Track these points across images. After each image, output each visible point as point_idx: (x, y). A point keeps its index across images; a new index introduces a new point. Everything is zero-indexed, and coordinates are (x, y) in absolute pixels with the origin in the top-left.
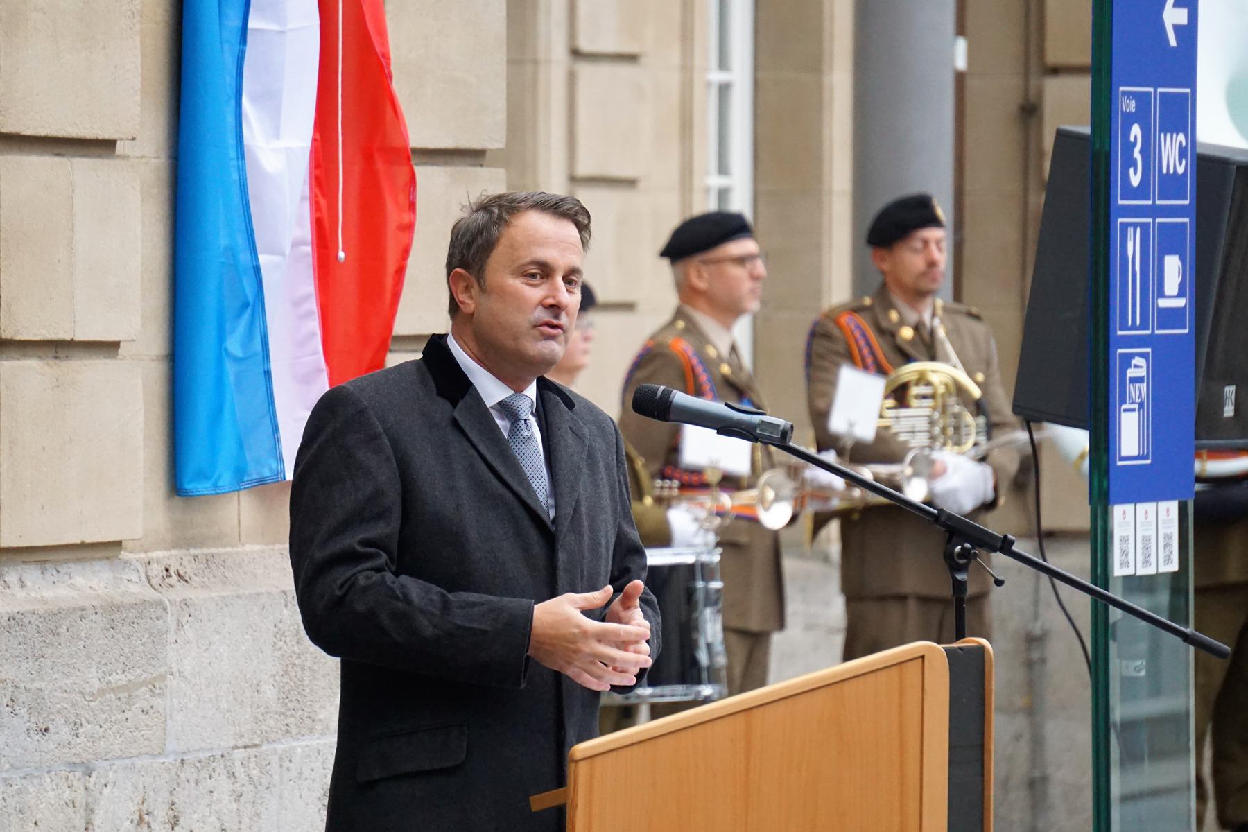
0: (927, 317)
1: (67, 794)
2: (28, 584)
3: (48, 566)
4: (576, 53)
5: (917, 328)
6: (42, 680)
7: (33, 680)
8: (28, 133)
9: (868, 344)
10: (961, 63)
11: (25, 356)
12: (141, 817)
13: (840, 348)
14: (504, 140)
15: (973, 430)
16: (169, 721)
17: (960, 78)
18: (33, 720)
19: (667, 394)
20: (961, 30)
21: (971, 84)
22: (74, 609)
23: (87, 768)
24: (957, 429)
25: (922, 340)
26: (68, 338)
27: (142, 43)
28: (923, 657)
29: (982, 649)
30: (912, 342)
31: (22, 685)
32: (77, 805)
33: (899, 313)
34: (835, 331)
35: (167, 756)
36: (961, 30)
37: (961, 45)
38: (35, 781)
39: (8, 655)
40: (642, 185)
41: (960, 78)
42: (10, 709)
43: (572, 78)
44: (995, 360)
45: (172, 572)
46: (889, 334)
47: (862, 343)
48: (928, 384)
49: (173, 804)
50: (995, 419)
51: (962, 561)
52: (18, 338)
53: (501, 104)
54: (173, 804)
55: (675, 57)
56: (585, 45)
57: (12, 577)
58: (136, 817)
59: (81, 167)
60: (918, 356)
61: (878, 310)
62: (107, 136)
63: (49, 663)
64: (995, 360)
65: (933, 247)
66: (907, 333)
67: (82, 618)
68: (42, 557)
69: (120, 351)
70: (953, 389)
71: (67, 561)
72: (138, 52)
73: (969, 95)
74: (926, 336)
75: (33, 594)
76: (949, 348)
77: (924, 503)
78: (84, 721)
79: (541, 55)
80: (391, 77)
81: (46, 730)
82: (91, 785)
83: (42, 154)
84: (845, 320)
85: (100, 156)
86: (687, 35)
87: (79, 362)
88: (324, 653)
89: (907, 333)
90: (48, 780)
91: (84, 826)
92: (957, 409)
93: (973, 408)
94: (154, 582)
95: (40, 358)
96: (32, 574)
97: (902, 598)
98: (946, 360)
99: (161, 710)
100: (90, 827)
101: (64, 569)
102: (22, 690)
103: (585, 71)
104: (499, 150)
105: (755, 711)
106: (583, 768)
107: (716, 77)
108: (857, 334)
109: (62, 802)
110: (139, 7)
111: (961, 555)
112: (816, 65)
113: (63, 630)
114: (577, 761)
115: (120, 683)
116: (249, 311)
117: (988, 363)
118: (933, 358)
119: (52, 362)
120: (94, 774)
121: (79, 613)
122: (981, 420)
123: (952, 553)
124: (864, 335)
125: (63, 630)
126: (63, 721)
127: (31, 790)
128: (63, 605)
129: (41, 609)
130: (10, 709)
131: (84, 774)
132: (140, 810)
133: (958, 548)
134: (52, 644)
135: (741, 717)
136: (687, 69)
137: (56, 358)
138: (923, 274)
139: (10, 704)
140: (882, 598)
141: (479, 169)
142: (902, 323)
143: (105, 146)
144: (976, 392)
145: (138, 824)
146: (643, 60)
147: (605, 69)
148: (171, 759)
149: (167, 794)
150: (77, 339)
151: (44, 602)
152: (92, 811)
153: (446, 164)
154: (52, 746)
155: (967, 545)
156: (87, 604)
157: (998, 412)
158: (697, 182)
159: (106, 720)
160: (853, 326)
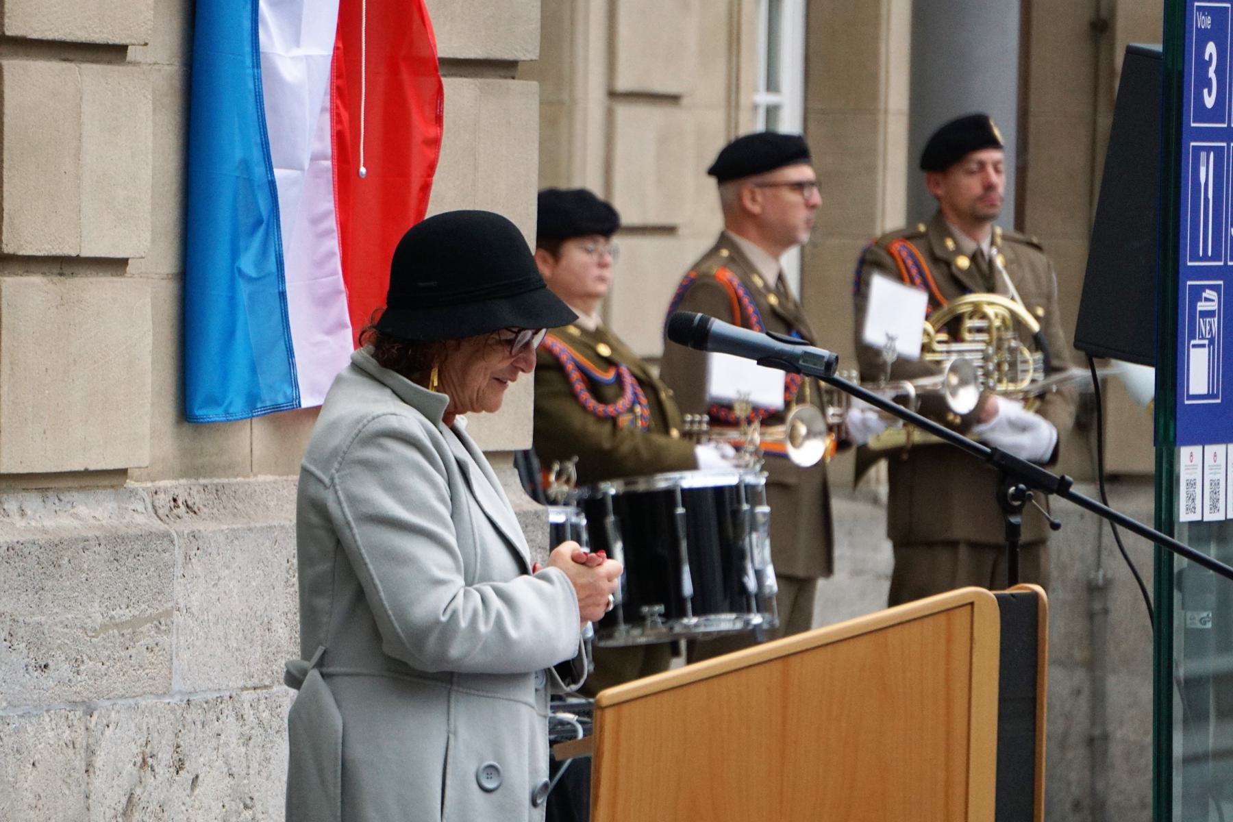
0: (985, 246)
1: (67, 735)
2: (29, 512)
3: (50, 494)
6: (42, 613)
8: (35, 36)
11: (27, 272)
12: (144, 760)
15: (1031, 367)
19: (704, 323)
23: (88, 707)
26: (74, 254)
28: (972, 604)
29: (1035, 596)
30: (968, 272)
31: (21, 619)
32: (77, 746)
35: (172, 696)
38: (34, 720)
39: (7, 586)
40: (684, 101)
50: (1055, 363)
51: (1017, 503)
52: (21, 253)
57: (11, 505)
58: (139, 760)
59: (90, 73)
62: (117, 41)
63: (50, 596)
65: (991, 170)
70: (1009, 322)
71: (69, 489)
74: (985, 267)
75: (33, 523)
78: (85, 658)
81: (46, 666)
82: (92, 726)
83: (49, 59)
84: (897, 247)
85: (109, 62)
89: (963, 262)
90: (48, 719)
91: (84, 768)
92: (1013, 344)
93: (1031, 340)
94: (161, 512)
95: (44, 274)
96: (32, 503)
97: (953, 544)
98: (1004, 292)
100: (91, 770)
101: (66, 497)
106: (609, 716)
111: (1016, 496)
114: (602, 709)
117: (1049, 298)
118: (991, 289)
119: (56, 279)
121: (82, 544)
122: (1039, 356)
123: (1005, 493)
124: (917, 264)
127: (29, 729)
128: (65, 535)
129: (42, 539)
131: (85, 713)
132: (143, 753)
133: (1012, 489)
134: (53, 576)
137: (61, 274)
139: (9, 638)
141: (510, 81)
142: (959, 251)
143: (114, 52)
144: (1035, 326)
148: (177, 698)
151: (46, 532)
153: (475, 75)
154: (52, 684)
155: (1022, 486)
158: (744, 100)
159: (109, 657)
160: (904, 254)
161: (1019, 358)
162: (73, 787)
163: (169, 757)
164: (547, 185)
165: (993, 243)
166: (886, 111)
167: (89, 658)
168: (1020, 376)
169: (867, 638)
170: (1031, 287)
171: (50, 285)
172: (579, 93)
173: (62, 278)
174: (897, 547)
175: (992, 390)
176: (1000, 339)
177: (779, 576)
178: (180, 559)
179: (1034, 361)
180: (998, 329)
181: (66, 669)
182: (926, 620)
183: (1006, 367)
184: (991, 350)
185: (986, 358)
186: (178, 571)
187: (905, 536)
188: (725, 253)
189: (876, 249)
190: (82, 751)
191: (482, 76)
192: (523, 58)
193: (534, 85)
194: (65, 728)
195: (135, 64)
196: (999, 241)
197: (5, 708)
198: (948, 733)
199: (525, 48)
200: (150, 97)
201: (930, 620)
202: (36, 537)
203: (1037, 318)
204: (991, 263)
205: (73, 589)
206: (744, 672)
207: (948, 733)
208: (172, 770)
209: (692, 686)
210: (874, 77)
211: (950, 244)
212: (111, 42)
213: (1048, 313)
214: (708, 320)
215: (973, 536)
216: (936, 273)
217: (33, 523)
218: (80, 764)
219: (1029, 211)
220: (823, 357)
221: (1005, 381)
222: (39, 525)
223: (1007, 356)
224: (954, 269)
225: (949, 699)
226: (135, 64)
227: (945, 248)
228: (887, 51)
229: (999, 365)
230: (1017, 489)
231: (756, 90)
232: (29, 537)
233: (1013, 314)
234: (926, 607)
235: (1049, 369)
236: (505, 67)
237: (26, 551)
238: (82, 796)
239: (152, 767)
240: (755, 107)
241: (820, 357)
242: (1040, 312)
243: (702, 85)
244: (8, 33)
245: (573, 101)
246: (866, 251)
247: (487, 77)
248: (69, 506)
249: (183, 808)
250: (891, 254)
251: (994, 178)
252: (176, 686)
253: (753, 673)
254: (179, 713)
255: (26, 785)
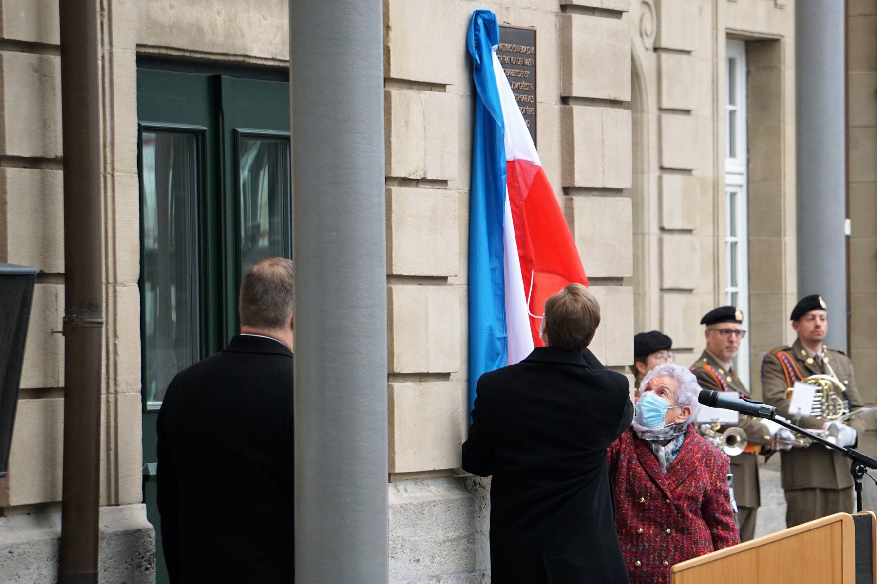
4: (662, 229)
9: (792, 366)
10: (848, 231)
11: (405, 381)
15: (842, 407)
19: (715, 395)
20: (848, 216)
24: (834, 406)
25: (817, 364)
26: (426, 372)
29: (870, 516)
30: (812, 365)
34: (776, 360)
36: (848, 216)
37: (848, 223)
40: (694, 292)
41: (848, 238)
43: (661, 241)
44: (853, 374)
47: (788, 365)
48: (819, 385)
50: (854, 403)
53: (631, 256)
56: (667, 226)
59: (431, 290)
61: (796, 351)
62: (443, 275)
65: (818, 319)
67: (434, 506)
68: (415, 477)
70: (832, 387)
71: (427, 479)
74: (820, 363)
76: (829, 367)
79: (646, 231)
80: (6, 193)
83: (413, 284)
84: (780, 355)
85: (440, 285)
88: (156, 446)
89: (810, 361)
92: (834, 396)
97: (814, 489)
98: (829, 374)
101: (425, 482)
103: (667, 237)
106: (678, 576)
107: (730, 239)
108: (786, 361)
111: (859, 471)
112: (778, 233)
117: (849, 375)
118: (823, 373)
119: (418, 383)
122: (846, 401)
124: (790, 362)
125: (426, 512)
136: (716, 236)
138: (812, 332)
140: (804, 490)
142: (808, 356)
143: (442, 280)
146: (694, 232)
147: (676, 237)
151: (417, 498)
153: (604, 285)
154: (421, 568)
157: (855, 401)
158: (721, 291)
164: (637, 333)
165: (823, 352)
166: (786, 294)
172: (647, 289)
174: (786, 492)
176: (828, 395)
177: (738, 507)
178: (478, 510)
183: (831, 407)
184: (824, 400)
195: (451, 285)
196: (826, 351)
199: (626, 272)
203: (845, 385)
204: (822, 361)
210: (780, 279)
211: (804, 352)
213: (850, 382)
215: (823, 486)
219: (852, 336)
223: (831, 402)
225: (833, 564)
226: (451, 285)
229: (828, 406)
231: (727, 286)
232: (409, 501)
233: (833, 383)
234: (824, 521)
235: (851, 407)
240: (727, 293)
244: (394, 273)
245: (644, 293)
246: (766, 357)
251: (819, 322)
252: (477, 568)
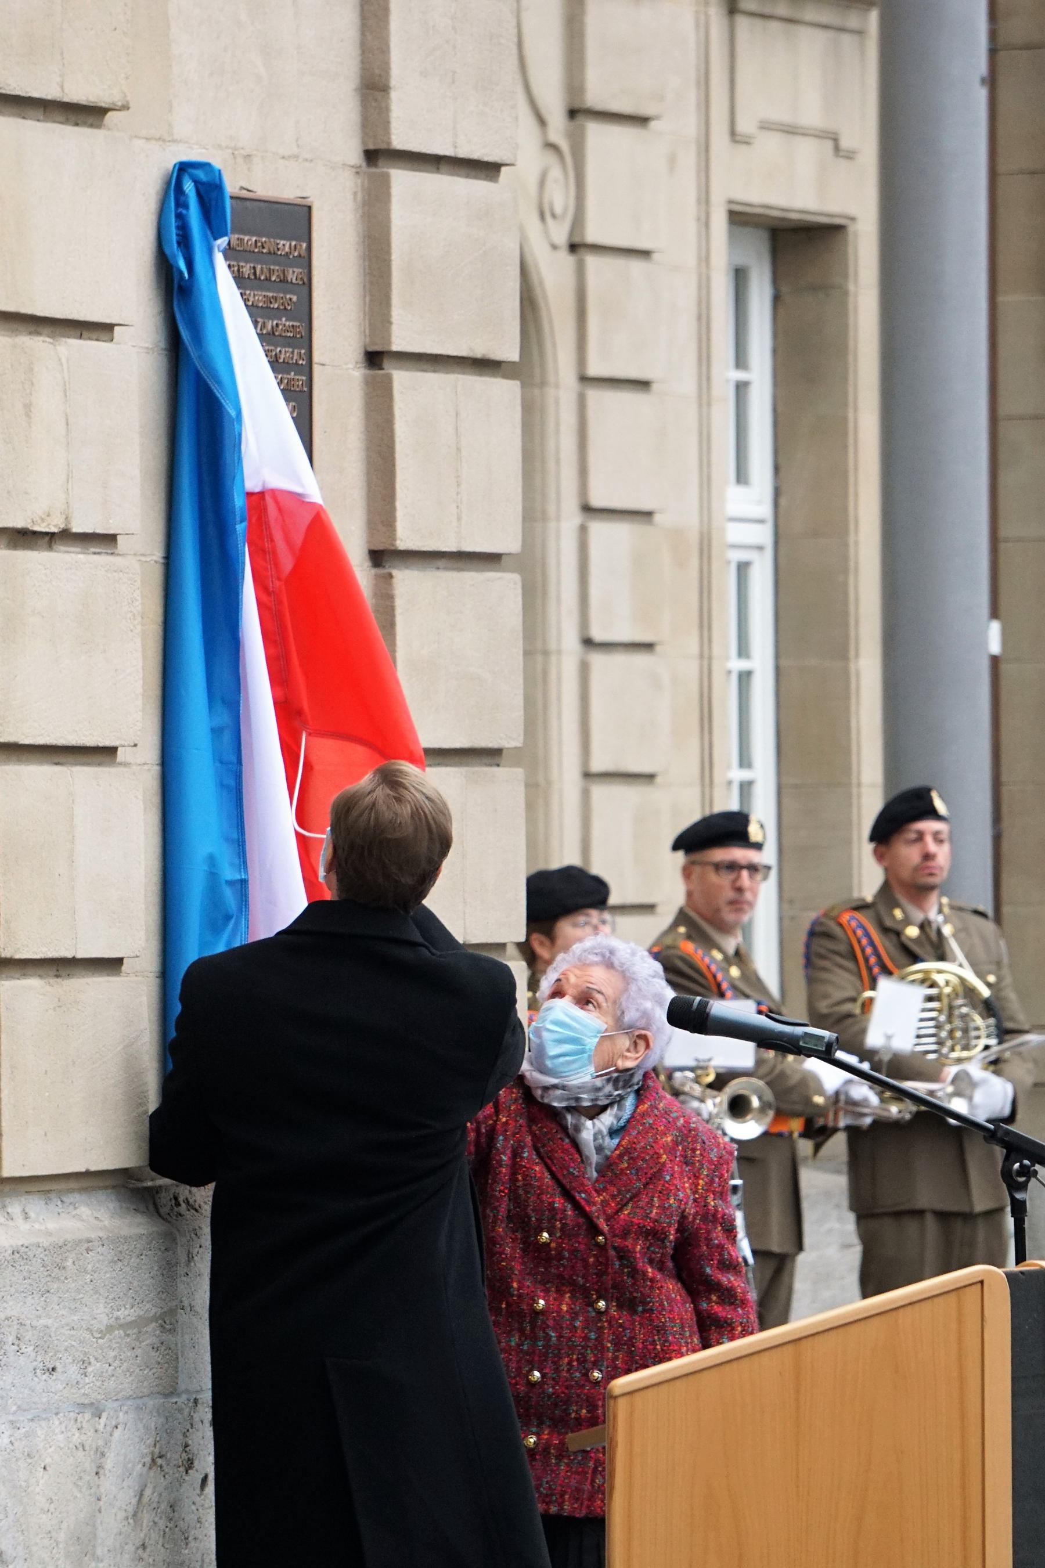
0: (933, 915)
1: (77, 1438)
2: (32, 1215)
3: (53, 1195)
4: (588, 642)
5: (924, 926)
6: (49, 1316)
7: (40, 1317)
8: (27, 742)
10: (995, 647)
11: (25, 975)
12: (153, 1460)
13: (842, 948)
14: (521, 738)
15: (983, 1033)
16: (180, 1359)
17: (995, 660)
18: (39, 1359)
19: (703, 1005)
20: (995, 613)
21: (1004, 667)
22: (80, 1241)
23: (97, 1408)
24: (966, 1031)
26: (69, 955)
27: (143, 645)
28: (982, 1282)
30: (917, 941)
31: (28, 1322)
32: (87, 1448)
33: (904, 912)
35: (179, 1395)
37: (995, 628)
38: (43, 1424)
39: (13, 1290)
40: (659, 780)
42: (16, 1348)
43: (584, 669)
44: (1006, 960)
45: (181, 1199)
46: (894, 933)
49: (187, 1446)
51: (1022, 1179)
52: (17, 956)
53: (519, 701)
54: (187, 1446)
55: (693, 645)
56: (598, 634)
57: (15, 1208)
58: (148, 1460)
60: (926, 957)
61: (882, 908)
62: (107, 743)
63: (55, 1299)
64: (1006, 960)
66: (912, 932)
67: (88, 1250)
68: (47, 1187)
69: (123, 968)
70: (960, 990)
71: (71, 1191)
72: (139, 655)
73: (1004, 683)
74: (933, 935)
75: (37, 1226)
76: (954, 945)
77: (988, 1121)
78: (92, 1360)
79: (552, 645)
81: (53, 1369)
82: (101, 1427)
83: (41, 763)
84: (845, 918)
85: (100, 765)
86: (705, 623)
87: (79, 980)
89: (912, 932)
90: (57, 1422)
91: (95, 1470)
92: (964, 1010)
93: (981, 1007)
94: (163, 1211)
95: (40, 976)
96: (35, 1206)
98: (954, 960)
99: (173, 1346)
100: (101, 1472)
101: (69, 1198)
102: (28, 1327)
103: (598, 660)
104: (516, 748)
105: (804, 1342)
106: (622, 1405)
107: (737, 665)
108: (859, 932)
109: (71, 1446)
110: (140, 608)
112: (841, 650)
113: (69, 1263)
114: (616, 1398)
115: (129, 1319)
116: (232, 922)
117: (999, 964)
118: (942, 957)
119: (53, 981)
120: (104, 1415)
121: (86, 1245)
122: (992, 1021)
123: (1011, 1170)
124: (867, 935)
125: (69, 1263)
126: (70, 1360)
127: (39, 1433)
128: (69, 1237)
129: (45, 1242)
130: (16, 1348)
131: (94, 1415)
132: (152, 1453)
133: (1017, 1165)
134: (58, 1279)
135: (789, 1348)
136: (706, 658)
137: (57, 976)
138: (917, 869)
139: (17, 1342)
140: (898, 1215)
141: (495, 769)
142: (907, 921)
143: (106, 753)
144: (986, 992)
145: (150, 1468)
148: (184, 1397)
149: (181, 1437)
150: (79, 956)
151: (49, 1234)
152: (103, 1455)
153: (460, 764)
154: (60, 1387)
155: (1026, 1162)
156: (93, 1235)
157: (1012, 1019)
158: (718, 778)
159: (115, 1357)
160: (854, 924)
161: (972, 1025)
162: (84, 1490)
163: (177, 1456)
165: (940, 911)
166: (859, 785)
167: (96, 1359)
168: (974, 1042)
169: (878, 1318)
170: (980, 952)
171: (48, 988)
173: (59, 980)
175: (946, 1057)
176: (951, 1008)
179: (987, 1027)
180: (949, 995)
181: (73, 1371)
182: (936, 1300)
183: (958, 1034)
185: (939, 1027)
186: (181, 1270)
187: (866, 1208)
188: (682, 930)
189: (824, 920)
190: (92, 1453)
191: (467, 765)
192: (507, 746)
193: (519, 772)
194: (74, 1430)
196: (946, 910)
197: (14, 1413)
198: (963, 1416)
199: (506, 734)
200: (141, 797)
201: (940, 1299)
202: (40, 1240)
203: (989, 985)
205: (78, 1291)
206: (755, 1356)
207: (963, 1416)
208: (182, 1469)
209: (705, 1373)
211: (898, 913)
212: (101, 745)
213: (1000, 979)
214: (707, 1003)
216: (888, 944)
217: (37, 1226)
218: (89, 1466)
220: (823, 1038)
221: (958, 1047)
222: (43, 1228)
223: (958, 1023)
224: (903, 939)
225: (962, 1379)
227: (893, 916)
228: (559, 673)
229: (951, 1032)
230: (1022, 1165)
231: (729, 767)
233: (962, 980)
236: (490, 755)
237: (31, 1254)
238: (93, 1499)
239: (161, 1466)
241: (821, 1038)
242: (991, 978)
243: (678, 767)
245: (549, 783)
246: (816, 923)
247: (473, 766)
248: (71, 1207)
249: (194, 1507)
250: (841, 925)
252: (182, 1386)
253: (765, 1358)
254: (186, 1411)
255: (38, 1489)
